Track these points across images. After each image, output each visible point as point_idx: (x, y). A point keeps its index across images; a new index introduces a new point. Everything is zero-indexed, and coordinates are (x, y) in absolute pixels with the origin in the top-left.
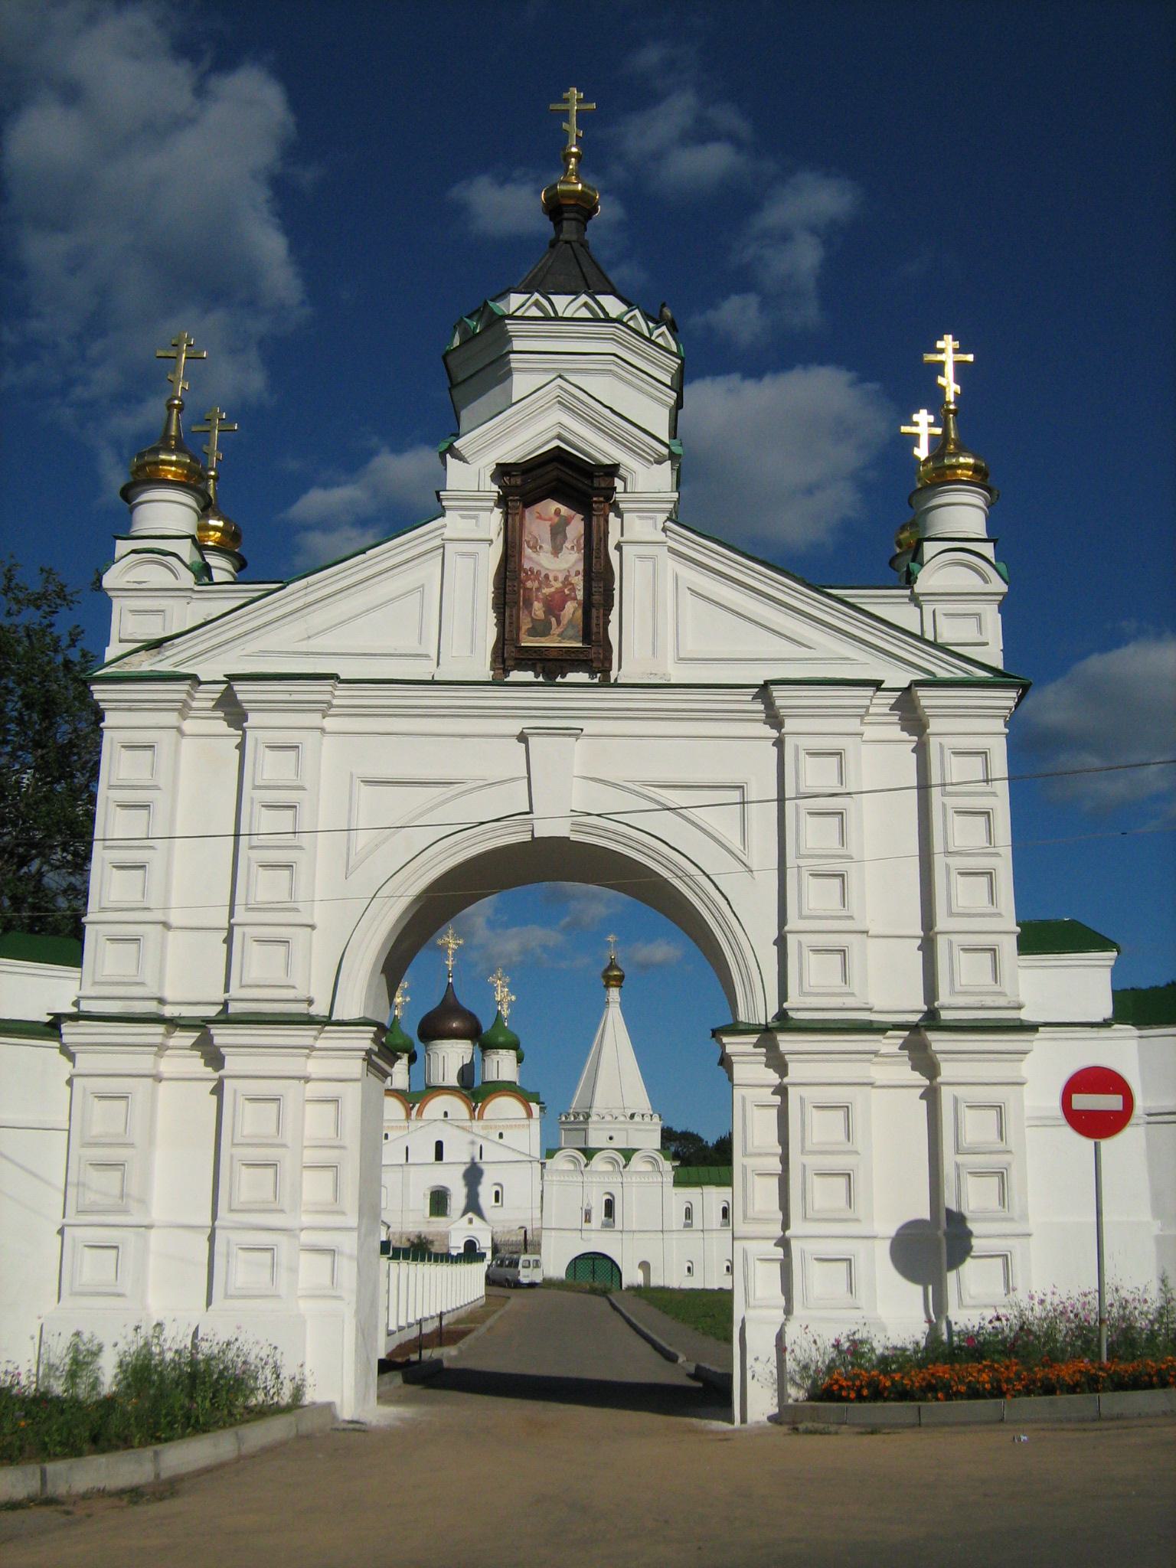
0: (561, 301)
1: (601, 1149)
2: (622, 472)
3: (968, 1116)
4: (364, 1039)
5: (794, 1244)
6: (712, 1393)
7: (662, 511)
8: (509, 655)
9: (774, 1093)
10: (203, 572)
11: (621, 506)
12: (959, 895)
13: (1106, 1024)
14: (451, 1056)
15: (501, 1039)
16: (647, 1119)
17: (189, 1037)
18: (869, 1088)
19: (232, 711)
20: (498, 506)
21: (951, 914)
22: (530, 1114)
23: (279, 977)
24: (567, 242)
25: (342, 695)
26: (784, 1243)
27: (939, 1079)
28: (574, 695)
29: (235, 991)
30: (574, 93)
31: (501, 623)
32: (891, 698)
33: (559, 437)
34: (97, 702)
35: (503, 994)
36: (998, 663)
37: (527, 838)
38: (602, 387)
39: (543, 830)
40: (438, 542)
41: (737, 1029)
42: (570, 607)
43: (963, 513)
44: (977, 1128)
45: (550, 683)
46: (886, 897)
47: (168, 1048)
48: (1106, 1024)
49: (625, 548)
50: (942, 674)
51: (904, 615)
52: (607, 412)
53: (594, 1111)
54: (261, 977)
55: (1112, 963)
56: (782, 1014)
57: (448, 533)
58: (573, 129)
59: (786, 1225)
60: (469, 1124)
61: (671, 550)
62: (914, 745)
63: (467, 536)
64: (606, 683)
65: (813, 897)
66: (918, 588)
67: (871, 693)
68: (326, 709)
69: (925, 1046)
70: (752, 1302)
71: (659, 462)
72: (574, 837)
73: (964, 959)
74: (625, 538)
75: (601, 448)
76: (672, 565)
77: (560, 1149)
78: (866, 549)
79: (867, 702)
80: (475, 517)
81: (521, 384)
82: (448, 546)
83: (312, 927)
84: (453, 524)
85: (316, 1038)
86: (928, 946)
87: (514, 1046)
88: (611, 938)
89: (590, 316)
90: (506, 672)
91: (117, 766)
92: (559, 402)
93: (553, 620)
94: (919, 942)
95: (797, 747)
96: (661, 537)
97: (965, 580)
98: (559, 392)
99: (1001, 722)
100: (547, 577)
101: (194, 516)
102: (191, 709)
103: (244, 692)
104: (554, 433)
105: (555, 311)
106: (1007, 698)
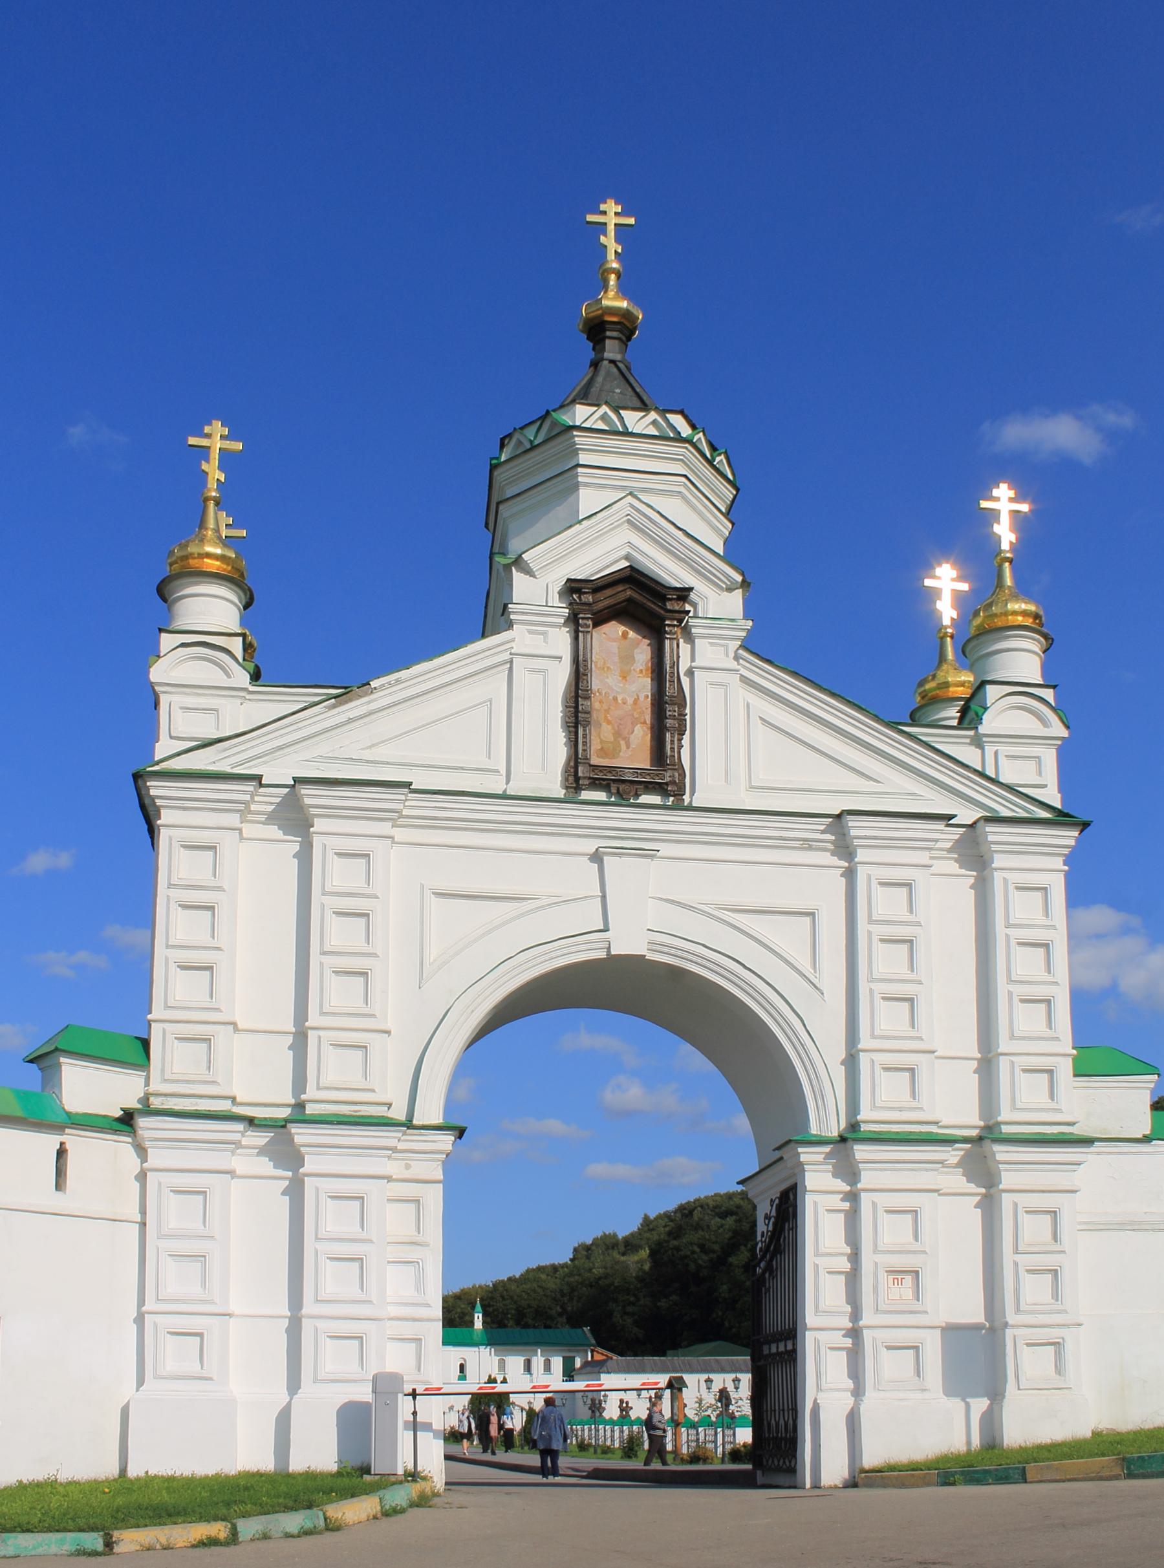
2: (692, 595)
3: (1026, 1220)
5: (867, 1335)
8: (585, 776)
9: (842, 1200)
11: (694, 630)
13: (1146, 1140)
17: (261, 1138)
19: (293, 816)
20: (566, 624)
21: (1012, 1037)
23: (356, 1080)
24: (612, 362)
25: (414, 806)
26: (855, 1333)
27: (859, 1186)
28: (645, 817)
29: (311, 1093)
31: (573, 743)
32: (955, 834)
34: (153, 798)
37: (602, 954)
38: (673, 508)
40: (506, 656)
42: (638, 728)
43: (1022, 659)
44: (1035, 1230)
46: (950, 1025)
48: (1146, 1140)
49: (697, 673)
52: (679, 534)
54: (334, 1078)
55: (1152, 1085)
56: (854, 1126)
59: (856, 1315)
61: (743, 679)
62: (972, 880)
64: (679, 806)
66: (982, 729)
67: (252, 789)
68: (396, 818)
69: (850, 1156)
70: (824, 1386)
71: (730, 590)
72: (650, 956)
75: (669, 570)
76: (743, 695)
78: (902, 684)
79: (248, 797)
80: (544, 633)
81: (588, 500)
82: (517, 661)
83: (388, 1032)
84: (519, 638)
85: (243, 1133)
89: (657, 434)
91: (176, 863)
92: (629, 521)
93: (622, 743)
94: (975, 1064)
95: (869, 877)
96: (733, 665)
97: (1026, 724)
98: (629, 510)
99: (1061, 860)
100: (615, 699)
102: (250, 812)
103: (311, 796)
104: (623, 553)
106: (1068, 837)
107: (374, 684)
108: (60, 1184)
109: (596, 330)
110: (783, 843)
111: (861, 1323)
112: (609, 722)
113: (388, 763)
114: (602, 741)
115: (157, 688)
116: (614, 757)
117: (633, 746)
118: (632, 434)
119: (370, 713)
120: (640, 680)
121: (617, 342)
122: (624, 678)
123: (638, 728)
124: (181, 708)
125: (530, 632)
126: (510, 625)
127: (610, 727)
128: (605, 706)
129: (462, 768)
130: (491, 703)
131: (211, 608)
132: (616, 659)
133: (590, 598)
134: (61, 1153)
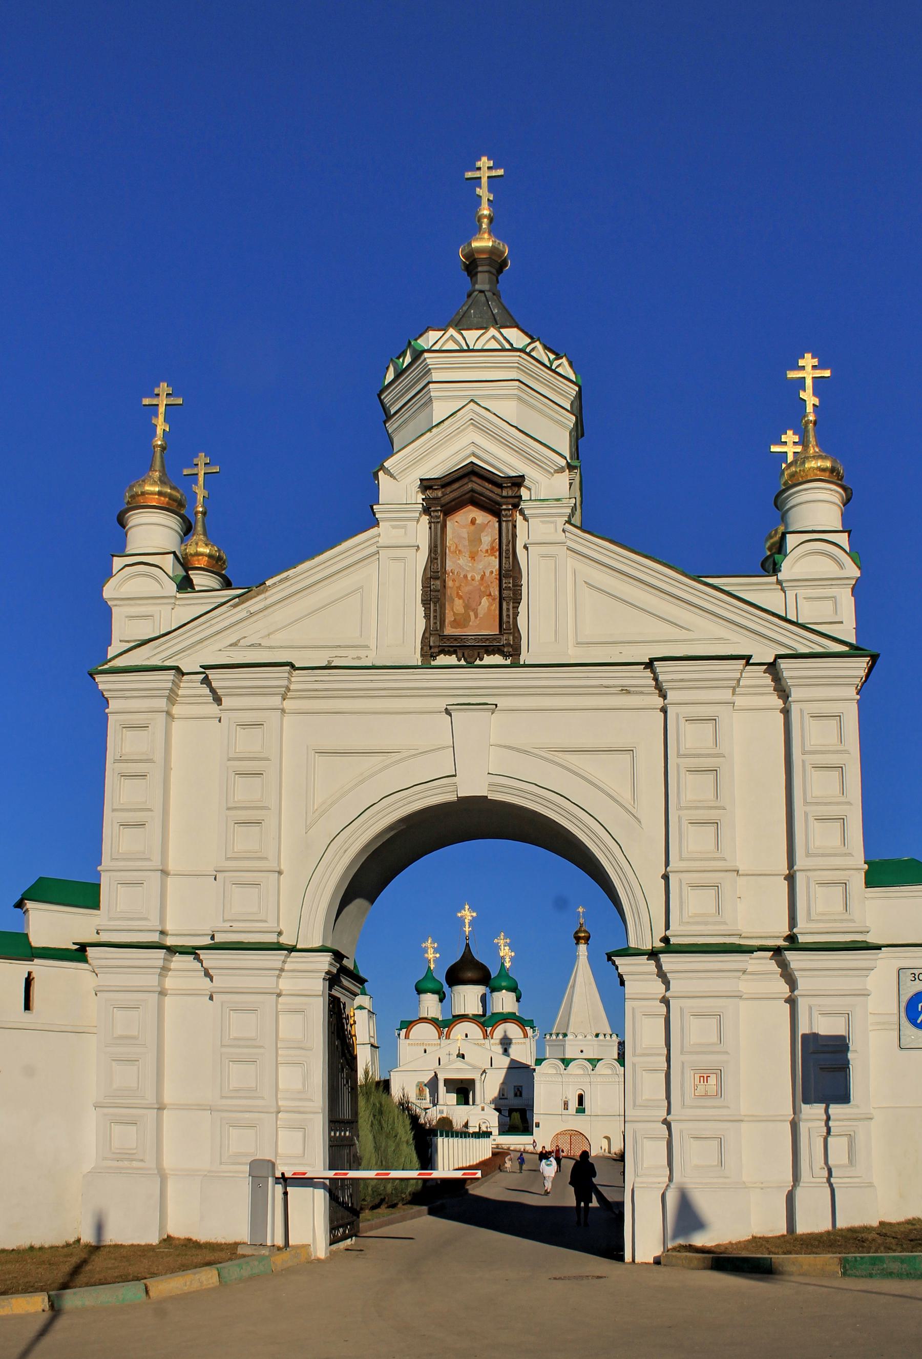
0: (471, 335)
1: (575, 1059)
2: (526, 483)
4: (324, 962)
6: (609, 1244)
7: (561, 515)
8: (440, 644)
10: (185, 584)
12: (816, 837)
14: (468, 998)
15: (504, 984)
16: (608, 1037)
18: (737, 1000)
22: (526, 1036)
24: (481, 291)
28: (491, 675)
30: (484, 162)
33: (474, 455)
35: (505, 952)
36: (853, 640)
37: (452, 798)
39: (466, 791)
40: (373, 549)
41: (627, 952)
42: (485, 601)
45: (470, 665)
46: (754, 841)
47: (170, 970)
50: (803, 650)
51: (770, 598)
53: (571, 1030)
56: (666, 940)
57: (382, 541)
58: (483, 192)
60: (483, 1041)
61: (569, 549)
63: (400, 530)
64: (515, 665)
65: (692, 842)
71: (557, 471)
73: (820, 892)
74: (531, 540)
75: (505, 462)
76: (572, 562)
77: (545, 1059)
80: (405, 527)
81: (440, 410)
84: (385, 532)
86: (791, 879)
87: (514, 989)
88: (581, 910)
90: (434, 657)
91: (120, 743)
93: (472, 614)
95: (677, 715)
96: (561, 537)
97: (824, 567)
100: (465, 577)
101: (178, 539)
104: (468, 452)
105: (511, 345)
106: (860, 665)
107: (268, 583)
108: (27, 1007)
109: (472, 266)
110: (605, 690)
111: (795, 868)
112: (460, 597)
113: (281, 647)
114: (455, 614)
115: (109, 603)
116: (465, 626)
117: (480, 615)
118: (473, 351)
119: (266, 608)
120: (486, 559)
121: (486, 274)
122: (473, 558)
123: (485, 601)
124: (127, 617)
125: (394, 527)
126: (376, 523)
127: (461, 601)
128: (457, 584)
129: (339, 646)
130: (366, 588)
131: (152, 531)
132: (466, 543)
133: (440, 494)
134: (29, 982)
